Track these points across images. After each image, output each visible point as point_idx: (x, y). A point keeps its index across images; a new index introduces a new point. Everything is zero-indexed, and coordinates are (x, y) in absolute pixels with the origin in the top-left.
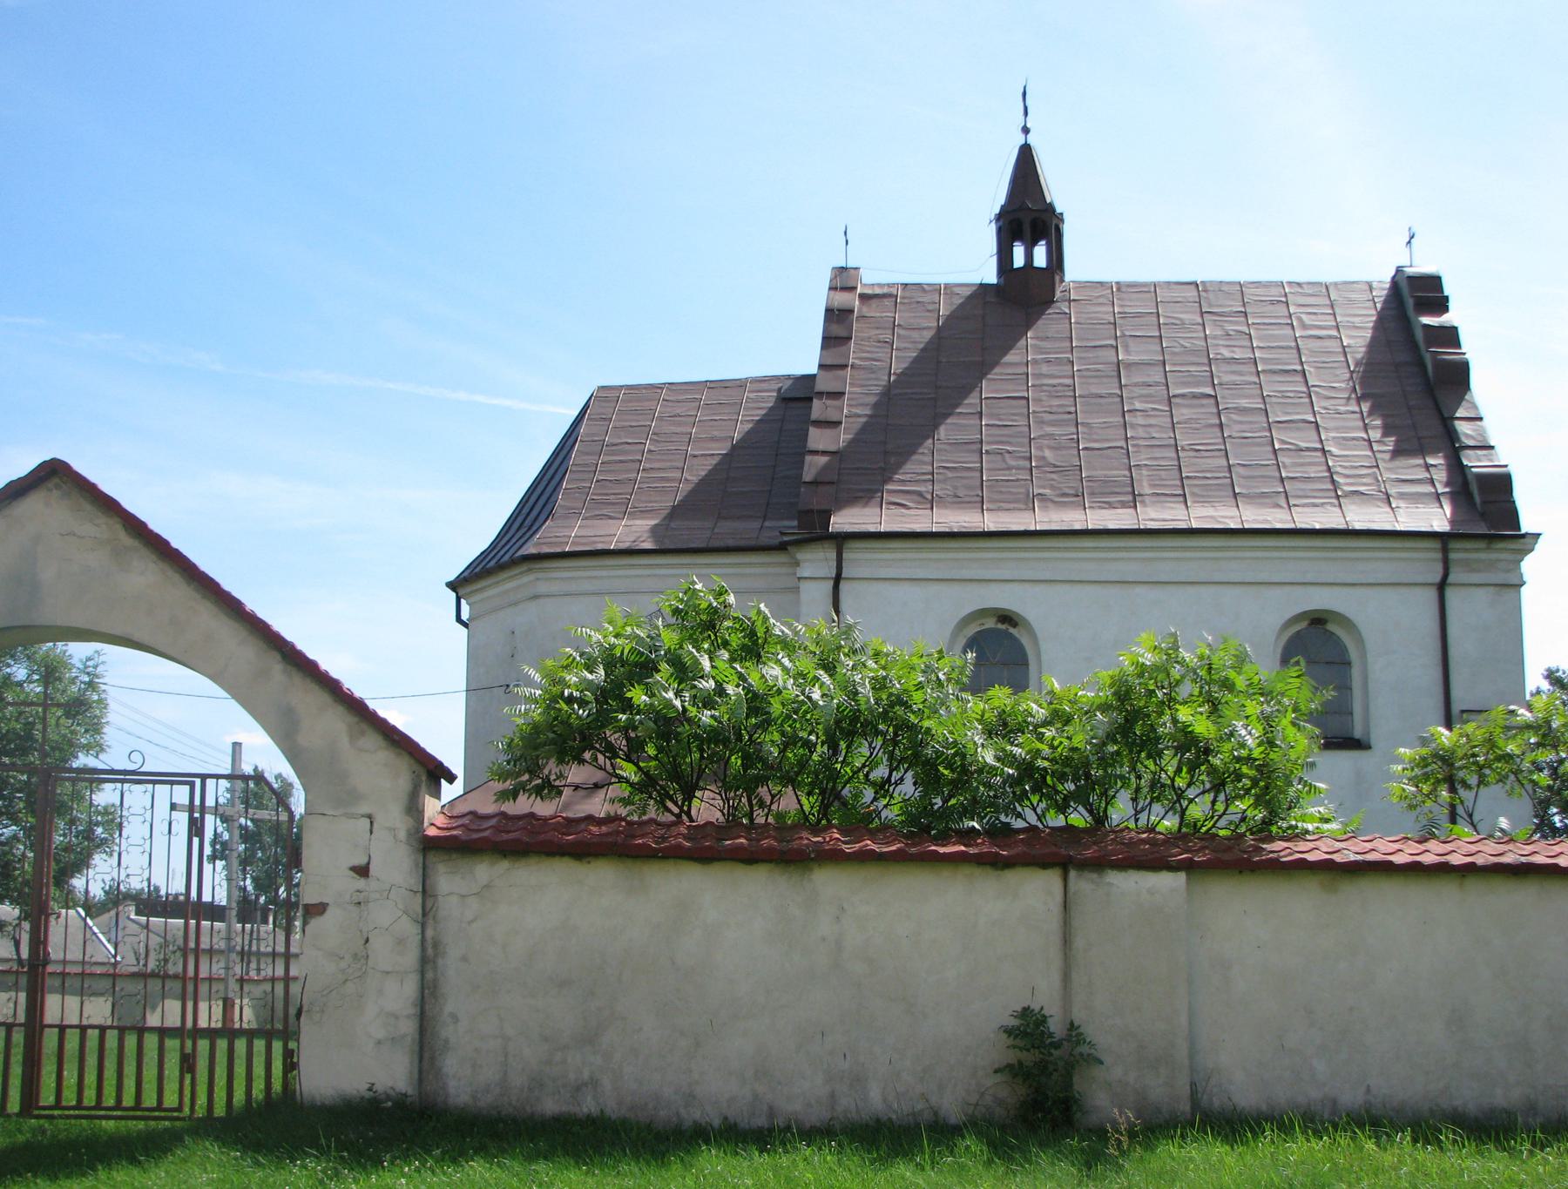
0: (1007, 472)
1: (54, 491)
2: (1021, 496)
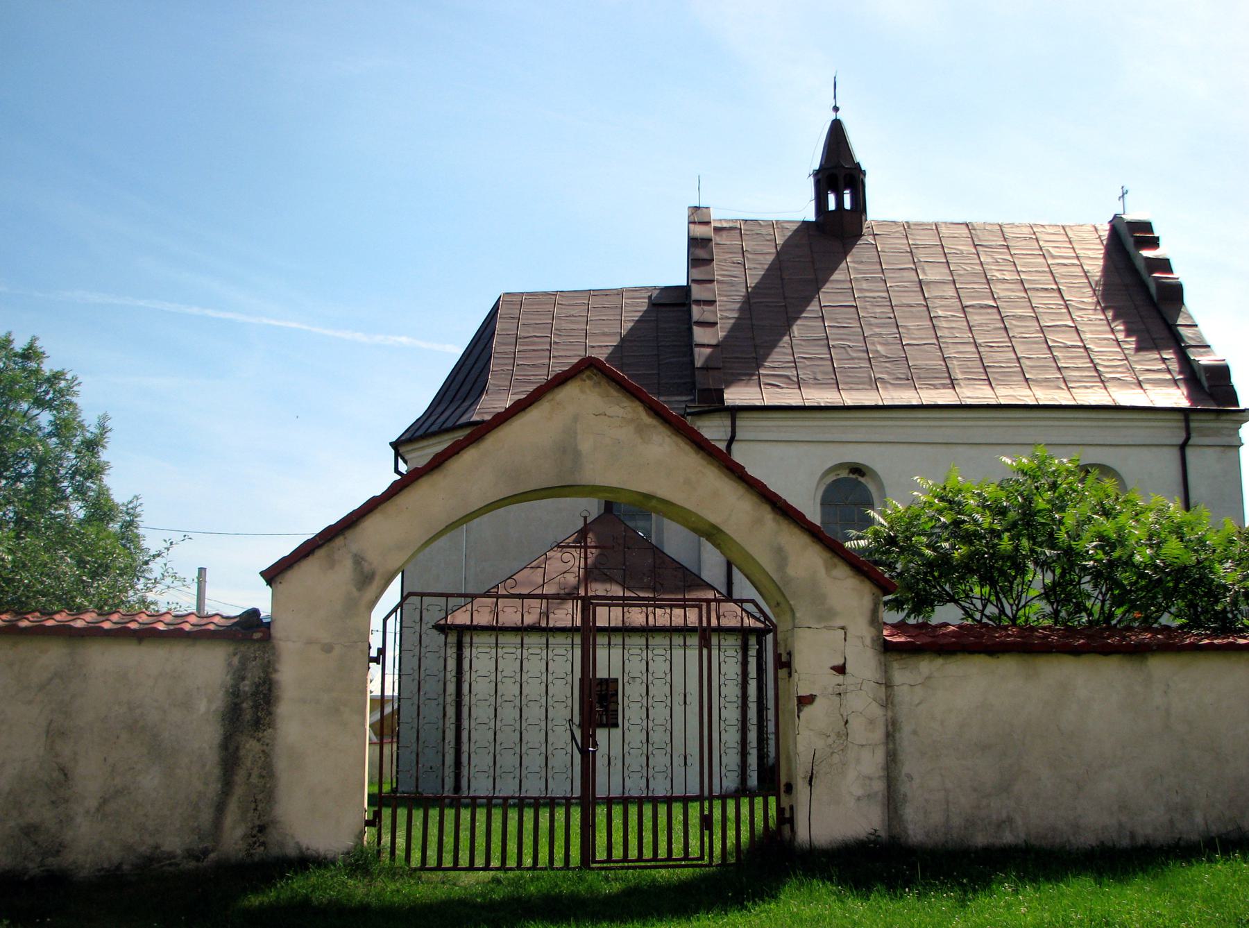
0: (851, 362)
1: (588, 381)
2: (866, 379)
